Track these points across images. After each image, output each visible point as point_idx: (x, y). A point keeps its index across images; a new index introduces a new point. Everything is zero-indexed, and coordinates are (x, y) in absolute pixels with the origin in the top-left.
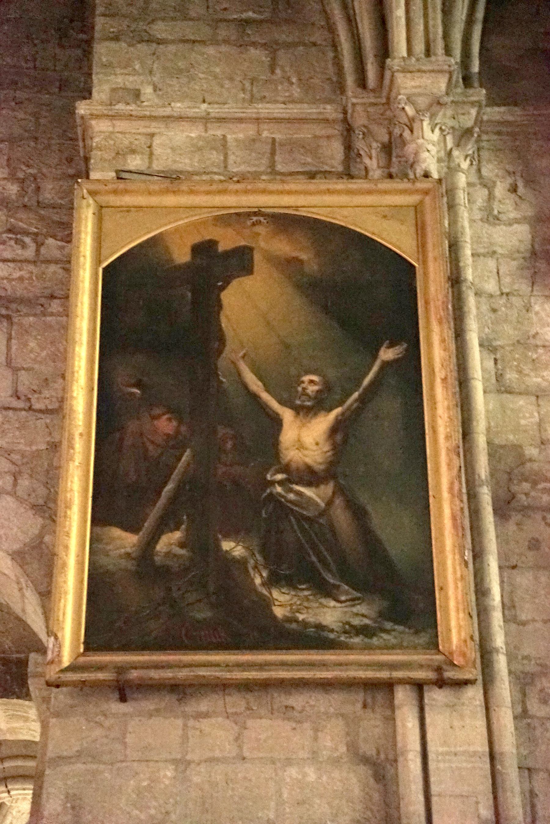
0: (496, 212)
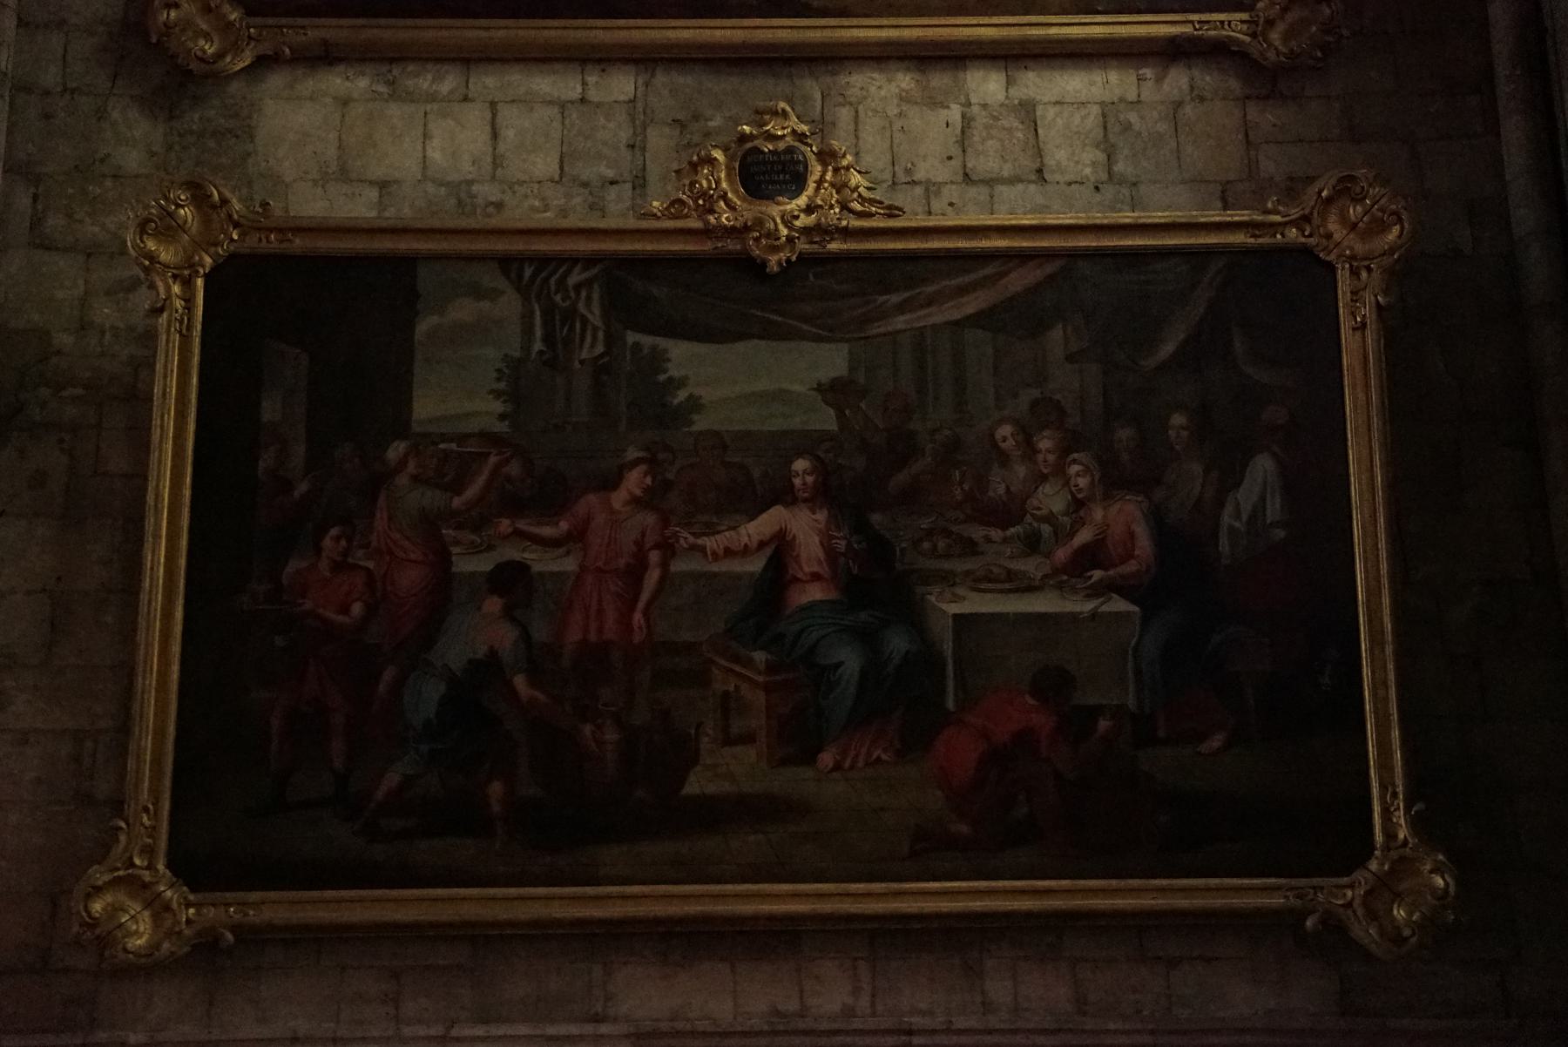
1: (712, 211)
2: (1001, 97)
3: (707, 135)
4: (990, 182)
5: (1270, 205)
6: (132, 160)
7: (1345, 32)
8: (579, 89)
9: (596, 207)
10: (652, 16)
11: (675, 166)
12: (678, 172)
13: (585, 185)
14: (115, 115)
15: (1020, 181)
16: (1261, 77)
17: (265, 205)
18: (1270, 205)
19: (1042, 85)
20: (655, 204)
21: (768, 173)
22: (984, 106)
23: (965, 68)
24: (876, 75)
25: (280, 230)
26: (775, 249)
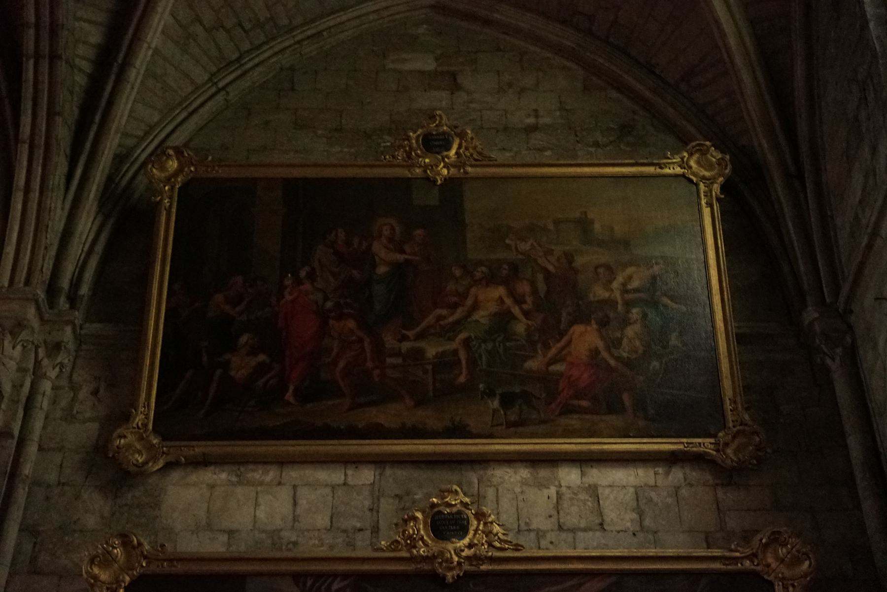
0: (75, 412)
1: (415, 547)
2: (578, 482)
3: (414, 502)
4: (573, 530)
5: (733, 547)
6: (91, 521)
7: (769, 450)
8: (343, 477)
9: (351, 545)
10: (385, 438)
11: (395, 521)
12: (396, 525)
13: (345, 531)
14: (85, 496)
15: (591, 530)
16: (726, 475)
17: (163, 546)
18: (733, 547)
19: (599, 476)
20: (383, 543)
21: (447, 525)
22: (569, 488)
23: (558, 467)
24: (508, 470)
25: (170, 561)
26: (451, 569)
